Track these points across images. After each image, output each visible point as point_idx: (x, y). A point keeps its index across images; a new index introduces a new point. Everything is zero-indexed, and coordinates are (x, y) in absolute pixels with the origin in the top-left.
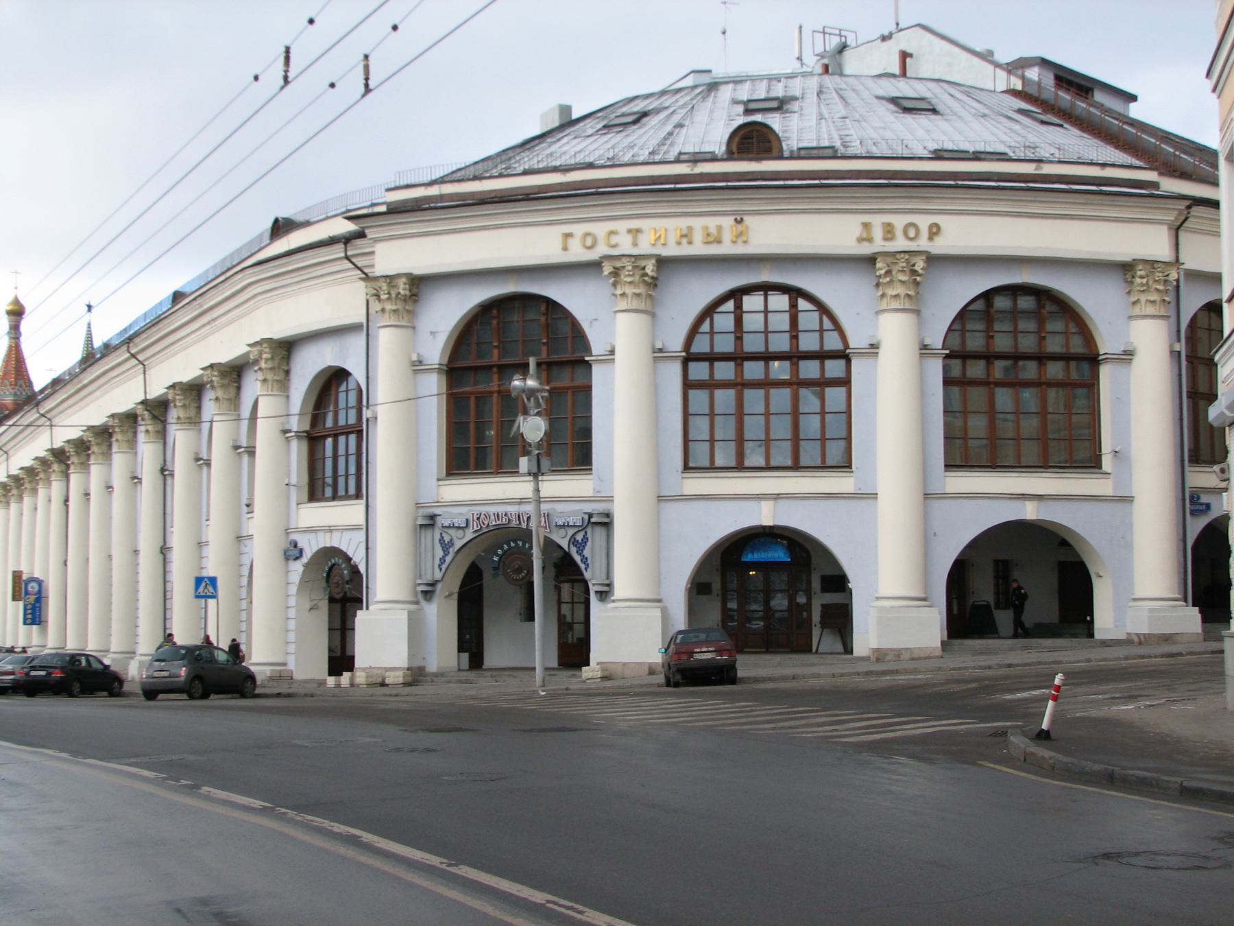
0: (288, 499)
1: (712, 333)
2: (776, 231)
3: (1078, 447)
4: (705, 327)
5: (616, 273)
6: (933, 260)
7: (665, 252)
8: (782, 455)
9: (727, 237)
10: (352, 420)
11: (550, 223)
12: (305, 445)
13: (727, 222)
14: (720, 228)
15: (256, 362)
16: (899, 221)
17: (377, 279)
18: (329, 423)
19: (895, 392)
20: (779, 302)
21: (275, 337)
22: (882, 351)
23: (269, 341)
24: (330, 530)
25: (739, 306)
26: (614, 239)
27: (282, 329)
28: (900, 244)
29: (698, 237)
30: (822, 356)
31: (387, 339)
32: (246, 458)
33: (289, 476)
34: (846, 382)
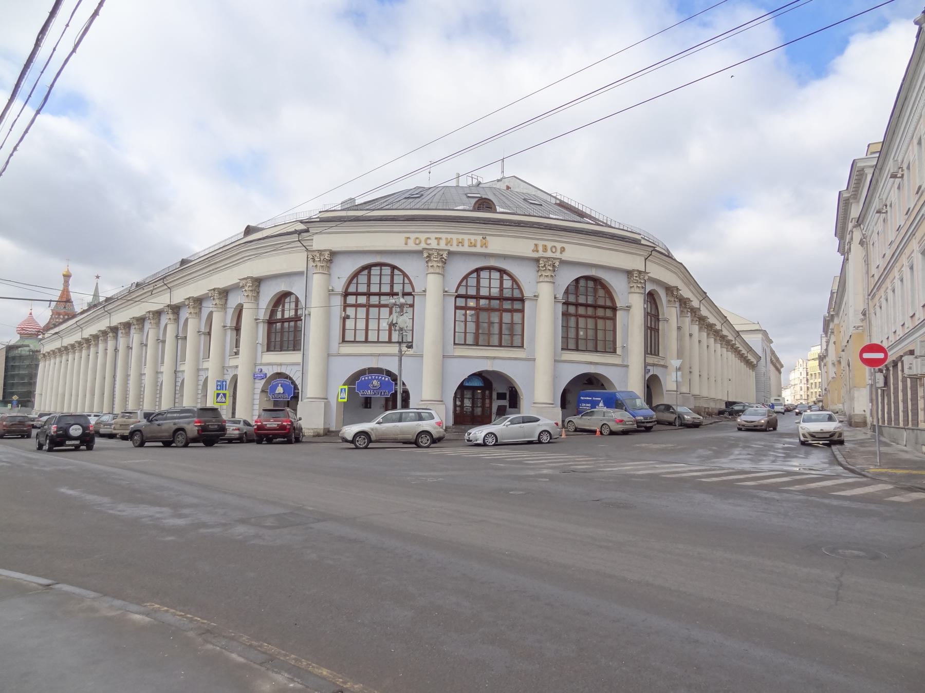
0: (256, 350)
1: (467, 286)
2: (500, 244)
3: (512, 337)
4: (355, 281)
5: (429, 256)
6: (563, 262)
7: (452, 249)
8: (495, 340)
9: (479, 245)
10: (292, 313)
11: (400, 232)
12: (266, 326)
13: (479, 238)
14: (476, 240)
15: (243, 287)
16: (549, 245)
17: (314, 251)
18: (279, 316)
19: (543, 318)
20: (496, 275)
21: (255, 276)
22: (539, 299)
23: (251, 278)
24: (281, 365)
25: (478, 276)
26: (429, 242)
27: (256, 274)
28: (549, 254)
29: (466, 244)
30: (513, 299)
31: (317, 280)
32: (160, 345)
33: (257, 339)
34: (522, 311)
